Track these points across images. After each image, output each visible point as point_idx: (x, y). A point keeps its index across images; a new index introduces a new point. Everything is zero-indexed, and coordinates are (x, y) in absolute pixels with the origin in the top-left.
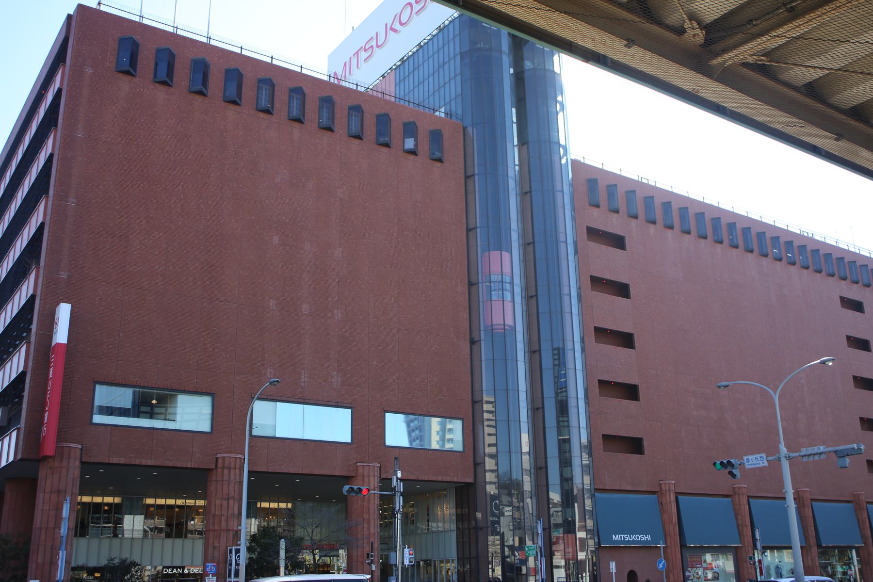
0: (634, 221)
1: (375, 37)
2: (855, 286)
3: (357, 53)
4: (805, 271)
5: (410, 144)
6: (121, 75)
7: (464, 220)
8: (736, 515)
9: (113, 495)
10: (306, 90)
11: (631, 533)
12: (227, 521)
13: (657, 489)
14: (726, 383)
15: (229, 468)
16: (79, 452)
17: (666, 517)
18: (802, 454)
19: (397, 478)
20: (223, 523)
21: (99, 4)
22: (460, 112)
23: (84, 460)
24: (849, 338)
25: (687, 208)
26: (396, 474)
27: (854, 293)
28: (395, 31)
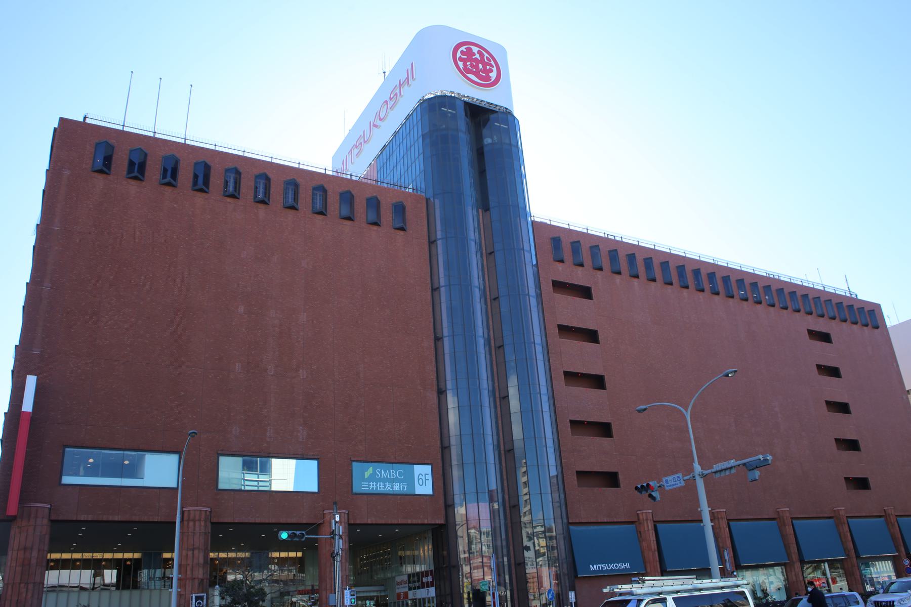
0: (599, 272)
2: (821, 319)
4: (772, 309)
6: (96, 174)
7: (429, 281)
9: (133, 551)
10: (270, 175)
12: (192, 570)
14: (644, 407)
15: (194, 521)
16: (47, 511)
17: (645, 544)
18: (714, 470)
19: (336, 522)
21: (85, 118)
22: (423, 186)
23: (53, 518)
24: (819, 367)
25: (651, 258)
27: (821, 326)
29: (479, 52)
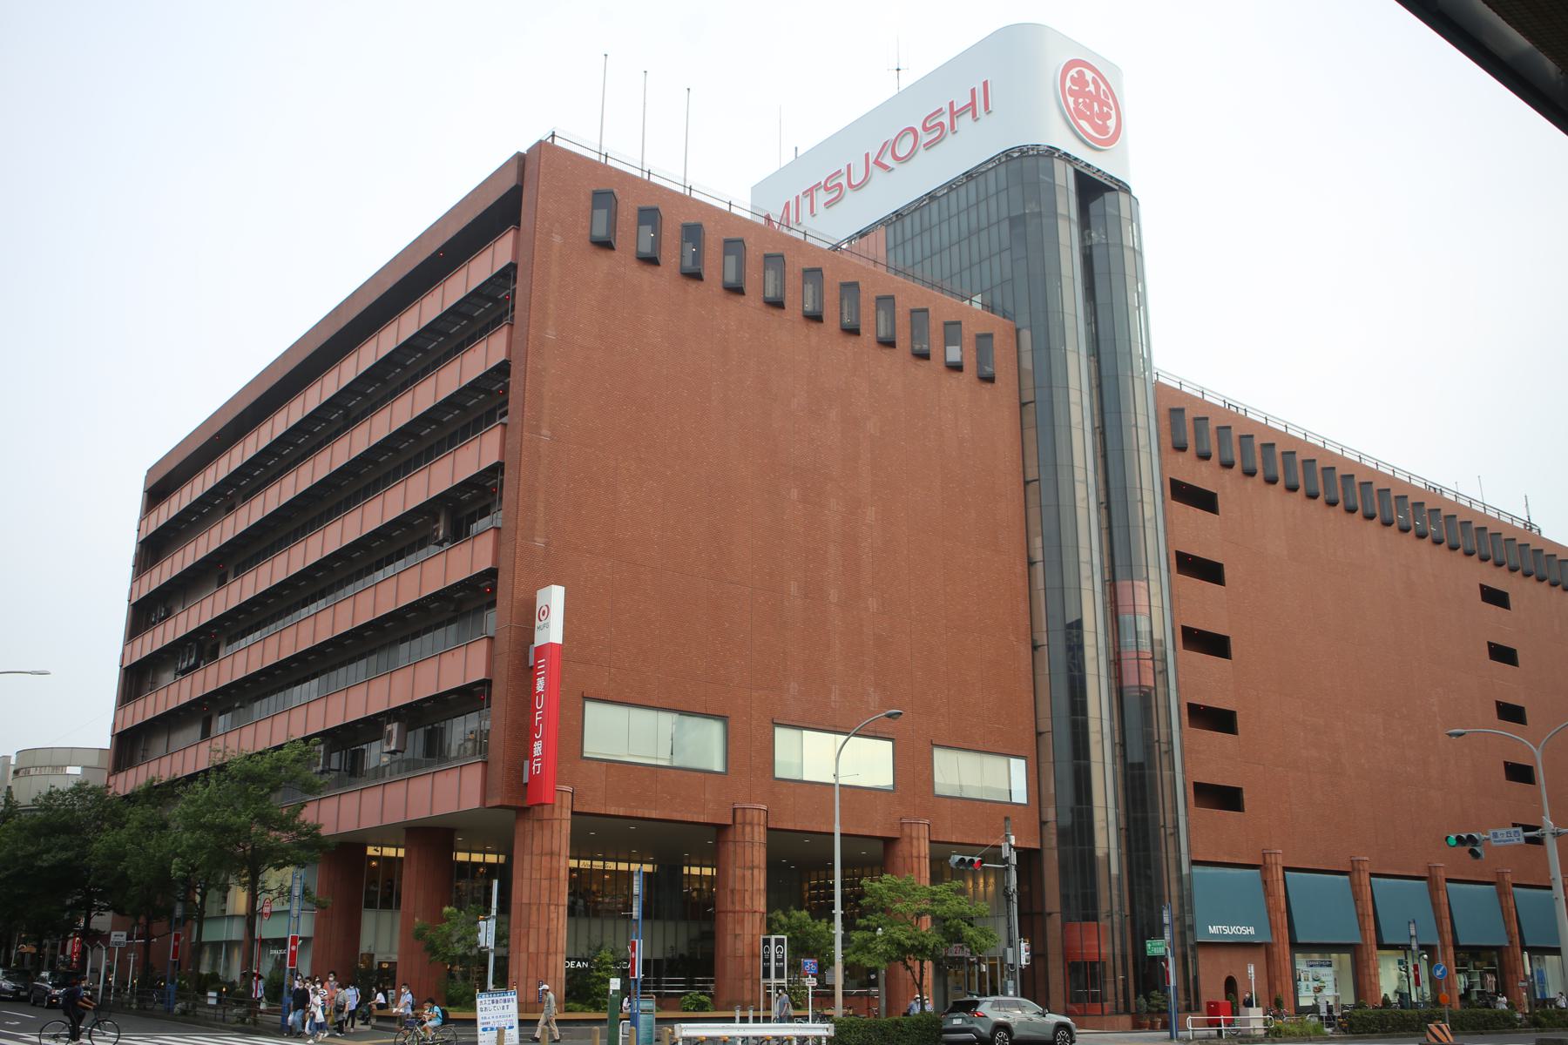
1: (844, 170)
3: (811, 190)
5: (954, 354)
8: (1356, 900)
16: (763, 814)
20: (748, 902)
27: (1499, 580)
28: (885, 167)
29: (1094, 81)
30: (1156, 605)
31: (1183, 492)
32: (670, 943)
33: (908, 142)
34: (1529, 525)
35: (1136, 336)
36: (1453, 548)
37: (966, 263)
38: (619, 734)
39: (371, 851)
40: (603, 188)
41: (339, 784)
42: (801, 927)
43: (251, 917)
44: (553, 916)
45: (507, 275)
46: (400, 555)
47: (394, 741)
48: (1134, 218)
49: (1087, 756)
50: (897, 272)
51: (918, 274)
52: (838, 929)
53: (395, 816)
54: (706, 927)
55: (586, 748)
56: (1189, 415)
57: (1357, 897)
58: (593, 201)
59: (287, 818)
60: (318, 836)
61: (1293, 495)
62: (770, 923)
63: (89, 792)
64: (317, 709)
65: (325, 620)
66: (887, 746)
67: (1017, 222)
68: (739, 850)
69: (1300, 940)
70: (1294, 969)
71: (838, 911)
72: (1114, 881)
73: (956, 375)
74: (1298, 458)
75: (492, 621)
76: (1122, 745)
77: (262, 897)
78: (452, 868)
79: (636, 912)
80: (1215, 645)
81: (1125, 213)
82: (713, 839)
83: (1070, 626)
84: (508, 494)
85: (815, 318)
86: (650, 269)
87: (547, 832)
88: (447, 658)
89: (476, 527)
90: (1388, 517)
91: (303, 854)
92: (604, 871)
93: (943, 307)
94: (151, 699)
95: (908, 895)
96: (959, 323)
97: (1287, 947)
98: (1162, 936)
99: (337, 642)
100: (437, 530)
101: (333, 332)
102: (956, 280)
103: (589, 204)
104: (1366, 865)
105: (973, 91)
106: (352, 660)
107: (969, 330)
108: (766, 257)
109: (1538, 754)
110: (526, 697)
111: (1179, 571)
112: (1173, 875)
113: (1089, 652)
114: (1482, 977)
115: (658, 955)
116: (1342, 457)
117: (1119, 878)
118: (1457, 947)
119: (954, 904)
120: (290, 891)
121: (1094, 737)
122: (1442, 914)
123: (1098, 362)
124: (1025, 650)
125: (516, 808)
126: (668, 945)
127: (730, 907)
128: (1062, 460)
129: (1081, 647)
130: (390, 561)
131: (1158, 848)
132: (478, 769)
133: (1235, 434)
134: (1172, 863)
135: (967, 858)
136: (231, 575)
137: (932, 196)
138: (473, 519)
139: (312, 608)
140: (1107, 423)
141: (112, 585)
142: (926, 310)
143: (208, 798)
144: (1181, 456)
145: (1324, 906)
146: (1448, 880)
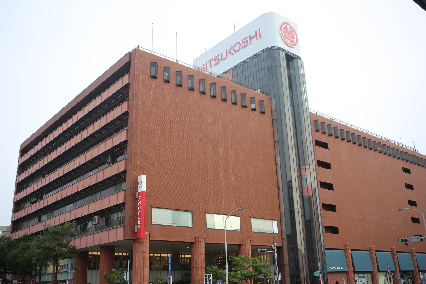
1: (220, 54)
3: (210, 60)
5: (253, 106)
11: (337, 266)
13: (344, 248)
20: (200, 264)
21: (139, 47)
23: (206, 242)
26: (274, 244)
27: (407, 166)
30: (312, 176)
31: (318, 143)
32: (176, 277)
33: (238, 46)
34: (415, 150)
35: (304, 100)
36: (394, 157)
37: (255, 80)
38: (162, 217)
39: (90, 253)
40: (153, 61)
41: (80, 234)
42: (215, 271)
43: (55, 274)
44: (145, 270)
45: (127, 86)
46: (97, 167)
47: (97, 221)
48: (302, 66)
49: (294, 219)
50: (236, 83)
51: (242, 83)
52: (227, 271)
53: (97, 243)
54: (187, 272)
55: (153, 221)
56: (319, 122)
57: (372, 258)
58: (151, 65)
59: (66, 244)
60: (75, 249)
61: (349, 143)
62: (206, 270)
63: (6, 239)
64: (73, 212)
65: (75, 186)
66: (238, 218)
67: (269, 68)
68: (197, 250)
69: (356, 270)
70: (355, 279)
71: (227, 266)
72: (303, 255)
73: (254, 112)
74: (350, 133)
75: (125, 185)
76: (304, 216)
77: (59, 268)
78: (116, 257)
79: (170, 268)
80: (329, 186)
81: (300, 65)
82: (189, 246)
83: (288, 182)
84: (129, 149)
85: (214, 97)
86: (167, 84)
87: (142, 246)
88: (112, 197)
89: (119, 159)
90: (376, 149)
91: (70, 255)
92: (157, 257)
93: (250, 93)
94: (23, 211)
95: (246, 261)
96: (255, 97)
97: (353, 272)
98: (318, 270)
99: (79, 193)
100: (108, 160)
101: (76, 104)
102: (253, 85)
103: (150, 66)
104: (374, 248)
105: (256, 32)
106: (83, 198)
107: (257, 99)
108: (200, 80)
109: (423, 215)
110: (135, 207)
111: (318, 166)
112: (320, 252)
113: (294, 190)
114: (408, 280)
115: (174, 281)
116: (357, 130)
117: (305, 254)
118: (400, 271)
119: (259, 263)
120: (67, 266)
121: (296, 214)
122: (396, 262)
123: (294, 107)
124: (276, 189)
125: (134, 239)
126: (176, 278)
127: (195, 266)
128: (285, 135)
129: (292, 188)
130: (94, 169)
131: (315, 245)
132: (122, 228)
133: (332, 126)
134: (319, 249)
135: (263, 250)
136: (46, 174)
137: (245, 62)
138: (118, 156)
139: (71, 183)
140: (297, 125)
141: (11, 178)
142: (245, 94)
143: (43, 239)
144: (317, 133)
145: (363, 260)
146: (397, 252)
